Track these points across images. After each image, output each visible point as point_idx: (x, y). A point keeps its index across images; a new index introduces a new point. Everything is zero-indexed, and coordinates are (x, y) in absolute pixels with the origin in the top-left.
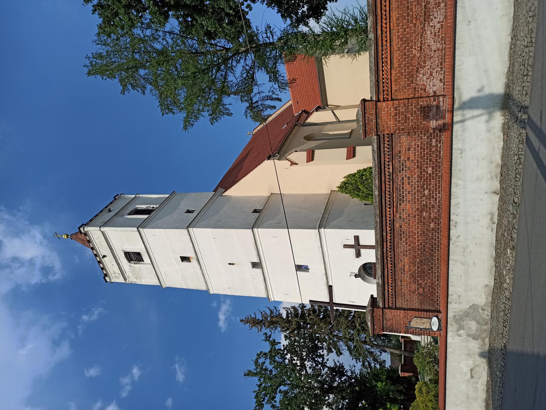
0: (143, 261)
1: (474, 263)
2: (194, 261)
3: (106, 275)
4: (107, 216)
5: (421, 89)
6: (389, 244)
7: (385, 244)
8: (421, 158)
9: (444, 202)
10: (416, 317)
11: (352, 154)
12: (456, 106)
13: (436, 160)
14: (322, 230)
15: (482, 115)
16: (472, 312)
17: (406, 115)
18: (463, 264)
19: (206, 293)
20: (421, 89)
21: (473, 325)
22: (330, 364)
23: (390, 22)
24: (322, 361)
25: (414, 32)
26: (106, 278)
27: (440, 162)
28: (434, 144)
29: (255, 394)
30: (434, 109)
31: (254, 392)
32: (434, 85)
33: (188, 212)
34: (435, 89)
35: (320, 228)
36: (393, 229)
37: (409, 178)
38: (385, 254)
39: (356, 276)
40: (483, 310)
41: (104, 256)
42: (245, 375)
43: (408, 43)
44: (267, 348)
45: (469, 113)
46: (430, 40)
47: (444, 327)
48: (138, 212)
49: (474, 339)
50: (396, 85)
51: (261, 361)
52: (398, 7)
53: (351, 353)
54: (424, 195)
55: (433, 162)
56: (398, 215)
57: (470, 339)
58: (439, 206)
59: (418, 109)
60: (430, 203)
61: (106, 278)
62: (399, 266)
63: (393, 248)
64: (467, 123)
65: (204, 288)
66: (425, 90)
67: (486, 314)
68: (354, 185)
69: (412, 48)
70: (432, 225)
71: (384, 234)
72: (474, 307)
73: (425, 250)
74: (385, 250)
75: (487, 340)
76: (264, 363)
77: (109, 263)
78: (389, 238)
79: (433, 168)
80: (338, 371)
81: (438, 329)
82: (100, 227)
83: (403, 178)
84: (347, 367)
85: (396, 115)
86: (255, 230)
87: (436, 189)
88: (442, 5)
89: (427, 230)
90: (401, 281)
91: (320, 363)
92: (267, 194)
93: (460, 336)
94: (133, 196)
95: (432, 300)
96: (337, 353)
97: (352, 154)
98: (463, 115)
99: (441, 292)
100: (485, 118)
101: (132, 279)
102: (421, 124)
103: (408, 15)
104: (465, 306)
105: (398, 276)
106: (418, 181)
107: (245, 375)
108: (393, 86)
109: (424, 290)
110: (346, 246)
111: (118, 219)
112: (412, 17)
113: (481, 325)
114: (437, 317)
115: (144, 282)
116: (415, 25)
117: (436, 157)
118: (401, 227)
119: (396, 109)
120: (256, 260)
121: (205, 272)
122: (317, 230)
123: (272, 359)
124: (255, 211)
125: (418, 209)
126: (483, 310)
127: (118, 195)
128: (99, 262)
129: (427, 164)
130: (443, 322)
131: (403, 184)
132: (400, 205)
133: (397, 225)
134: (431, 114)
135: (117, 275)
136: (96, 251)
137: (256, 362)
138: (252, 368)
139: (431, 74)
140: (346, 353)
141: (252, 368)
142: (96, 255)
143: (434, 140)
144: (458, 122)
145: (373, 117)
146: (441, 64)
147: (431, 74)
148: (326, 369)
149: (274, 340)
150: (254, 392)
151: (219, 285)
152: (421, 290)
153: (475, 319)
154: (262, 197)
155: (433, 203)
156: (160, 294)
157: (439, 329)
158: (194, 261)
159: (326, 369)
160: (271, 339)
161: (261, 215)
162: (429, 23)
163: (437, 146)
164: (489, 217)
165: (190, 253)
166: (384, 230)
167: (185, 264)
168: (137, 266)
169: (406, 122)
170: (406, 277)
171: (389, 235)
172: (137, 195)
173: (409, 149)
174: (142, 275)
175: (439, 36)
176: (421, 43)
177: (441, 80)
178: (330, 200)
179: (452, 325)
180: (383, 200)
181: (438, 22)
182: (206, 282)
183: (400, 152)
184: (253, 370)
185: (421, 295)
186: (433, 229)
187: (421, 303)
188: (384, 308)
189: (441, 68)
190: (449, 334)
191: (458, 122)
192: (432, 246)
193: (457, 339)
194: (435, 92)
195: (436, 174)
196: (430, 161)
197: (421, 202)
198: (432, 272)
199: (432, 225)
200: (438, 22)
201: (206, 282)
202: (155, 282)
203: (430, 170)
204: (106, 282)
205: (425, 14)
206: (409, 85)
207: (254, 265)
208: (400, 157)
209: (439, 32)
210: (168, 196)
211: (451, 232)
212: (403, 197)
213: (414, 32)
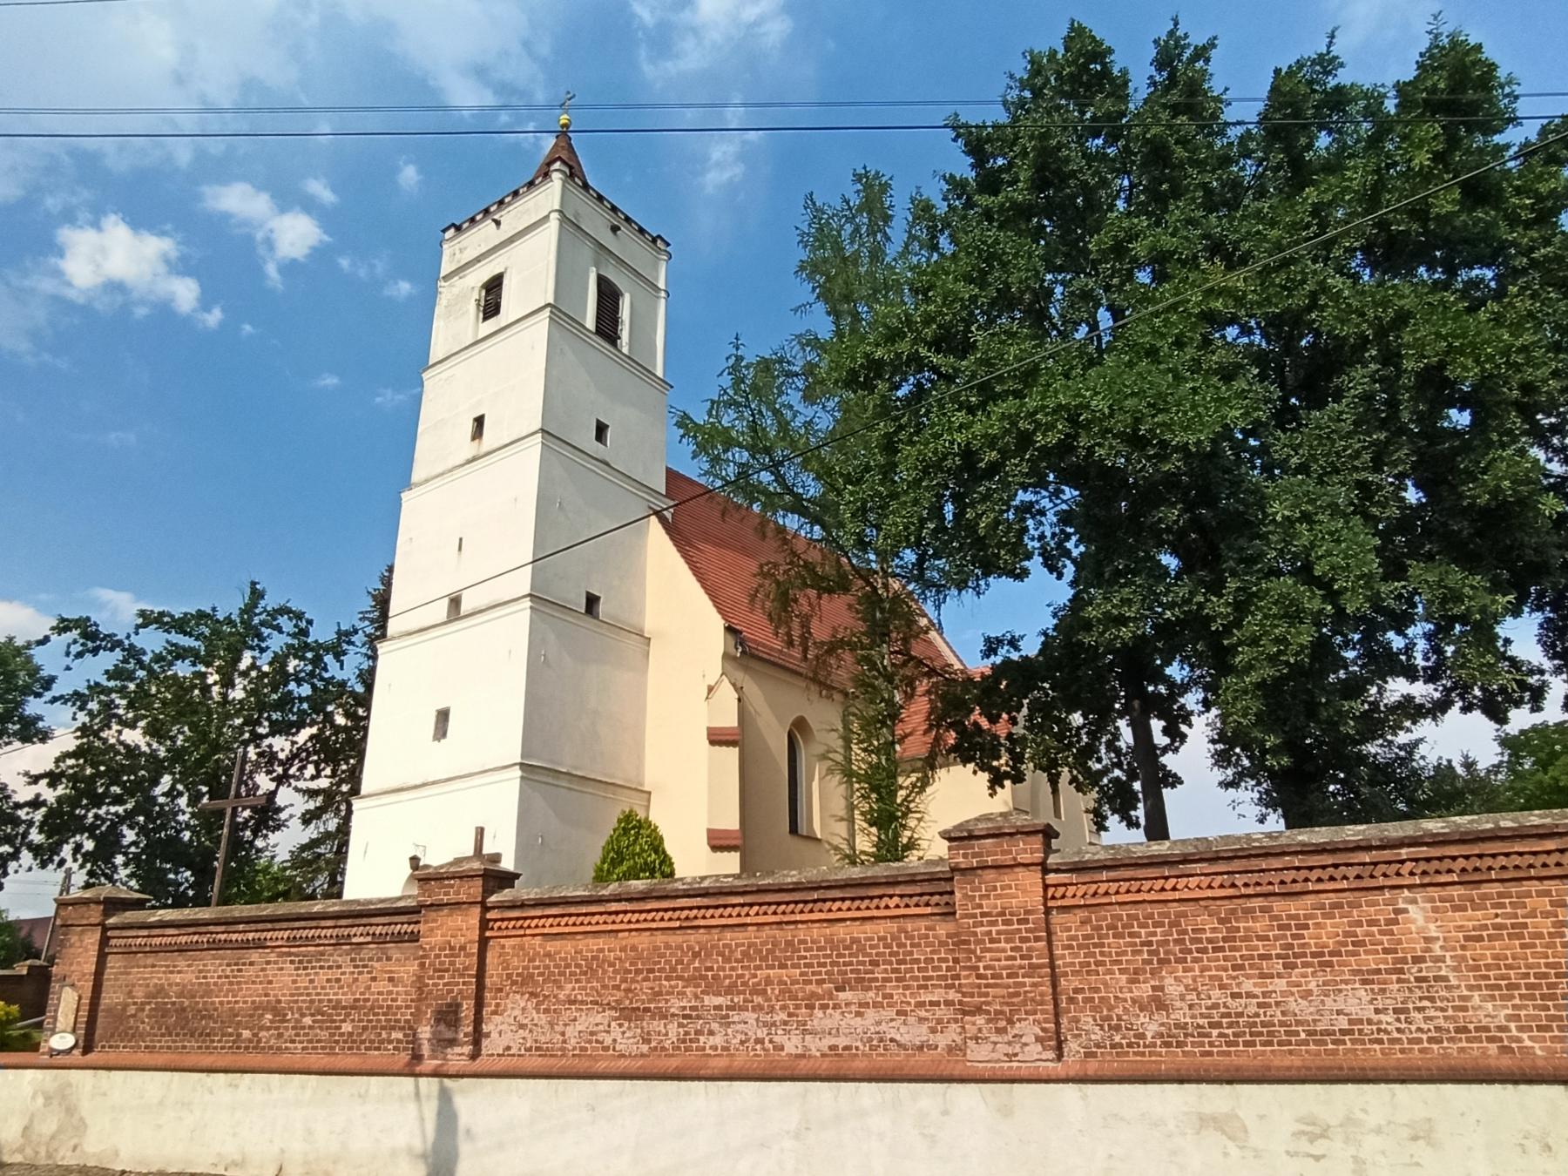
0: (485, 319)
1: (160, 1126)
2: (471, 449)
3: (458, 228)
4: (596, 223)
5: (498, 1005)
6: (223, 937)
7: (222, 928)
8: (372, 1008)
9: (284, 1060)
10: (80, 998)
11: (719, 842)
12: (446, 1081)
13: (363, 1042)
14: (517, 772)
15: (425, 1141)
16: (74, 1121)
17: (447, 970)
18: (161, 1103)
19: (405, 482)
20: (498, 1005)
21: (47, 1127)
22: (285, 796)
23: (630, 930)
24: (293, 776)
25: (604, 987)
26: (452, 230)
27: (359, 1048)
28: (394, 1035)
29: (209, 611)
30: (449, 1035)
31: (214, 609)
32: (501, 1034)
33: (601, 430)
34: (494, 1035)
35: (521, 764)
36: (246, 946)
37: (338, 980)
38: (203, 929)
39: (414, 861)
40: (75, 1148)
41: (498, 223)
42: (253, 584)
43: (585, 973)
44: (322, 633)
45: (431, 1109)
46: (587, 1021)
47: (59, 1060)
48: (608, 297)
49: (26, 1129)
50: (513, 947)
51: (283, 621)
52: (656, 948)
53: (303, 848)
54: (303, 1015)
55: (360, 1035)
56: (273, 957)
57: (25, 1122)
58: (279, 1048)
59: (455, 998)
60: (286, 1028)
61: (452, 230)
62: (182, 963)
63: (216, 946)
64: (412, 1107)
65: (415, 478)
66: (495, 1013)
67: (67, 1158)
68: (636, 849)
69: (577, 981)
70: (246, 1034)
71: (241, 927)
72: (82, 1127)
73: (203, 1017)
74: (211, 928)
75: (18, 1158)
76: (281, 632)
77: (484, 235)
78: (234, 937)
79: (351, 1034)
80: (267, 815)
81: (52, 1050)
82: (560, 211)
83: (339, 967)
84: (274, 838)
85: (452, 948)
86: (527, 603)
87: (310, 1041)
88: (645, 1048)
89: (239, 1023)
90: (153, 966)
91: (286, 771)
92: (649, 627)
93: (33, 1098)
94: (661, 285)
95: (112, 1035)
96: (308, 812)
97: (719, 842)
98: (429, 1097)
99: (125, 1055)
100: (418, 1145)
101: (447, 293)
102: (428, 1006)
103: (638, 972)
104: (85, 1107)
105: (162, 961)
106: (330, 1001)
107: (253, 584)
108: (512, 941)
109: (133, 1016)
110: (480, 832)
111: (587, 251)
112: (633, 981)
113: (48, 1144)
114: (75, 1046)
115: (438, 325)
116: (617, 987)
117: (372, 1042)
118: (252, 964)
119: (463, 948)
120: (465, 607)
121: (448, 477)
122: (519, 760)
123: (297, 652)
124: (592, 602)
125: (279, 1002)
126: (75, 1148)
127: (668, 245)
128: (486, 212)
129: (360, 1021)
130: (60, 1059)
131: (330, 968)
132: (292, 962)
133: (255, 955)
134: (442, 1027)
135: (458, 255)
136: (510, 204)
137: (284, 611)
138: (270, 602)
139: (522, 1026)
140: (312, 832)
141: (270, 602)
142: (501, 202)
143: (400, 1036)
144: (417, 1087)
145: (452, 898)
146: (538, 1049)
147: (522, 1026)
148: (272, 786)
149: (345, 653)
150: (214, 609)
151: (420, 513)
152: (132, 1010)
153: (59, 1131)
154: (642, 613)
155: (286, 1034)
156: (411, 363)
157: (53, 1053)
158: (471, 449)
159: (272, 786)
160: (345, 646)
161: (575, 615)
162: (616, 1019)
163: (390, 1042)
164: (237, 1157)
165: (490, 437)
166: (247, 927)
167: (469, 427)
168: (472, 306)
169: (435, 971)
170: (158, 978)
171: (240, 937)
172: (663, 294)
173: (391, 979)
174: (455, 317)
175: (590, 1042)
176: (582, 1002)
177: (509, 1048)
178: (620, 790)
179: (55, 1079)
180: (303, 924)
181: (615, 1041)
182: (427, 481)
183: (389, 959)
184: (262, 603)
185: (124, 1009)
186: (240, 1035)
187: (109, 1010)
188: (105, 929)
189: (530, 1049)
190: (39, 1074)
191: (417, 1087)
192: (208, 1035)
193: (28, 1090)
194: (488, 1035)
195: (337, 1042)
196: (365, 1028)
197: (291, 1009)
198: (163, 1035)
199: (246, 1034)
200: (615, 1041)
201: (427, 481)
202: (436, 353)
203: (347, 1027)
204: (444, 231)
205: (634, 1009)
206: (509, 976)
207: (455, 602)
208: (379, 960)
209: (597, 1041)
210: (659, 373)
211: (222, 1075)
212: (305, 968)
213: (604, 987)
